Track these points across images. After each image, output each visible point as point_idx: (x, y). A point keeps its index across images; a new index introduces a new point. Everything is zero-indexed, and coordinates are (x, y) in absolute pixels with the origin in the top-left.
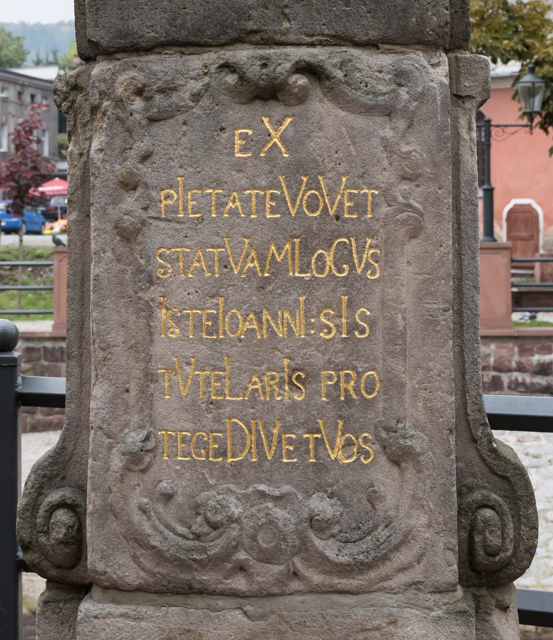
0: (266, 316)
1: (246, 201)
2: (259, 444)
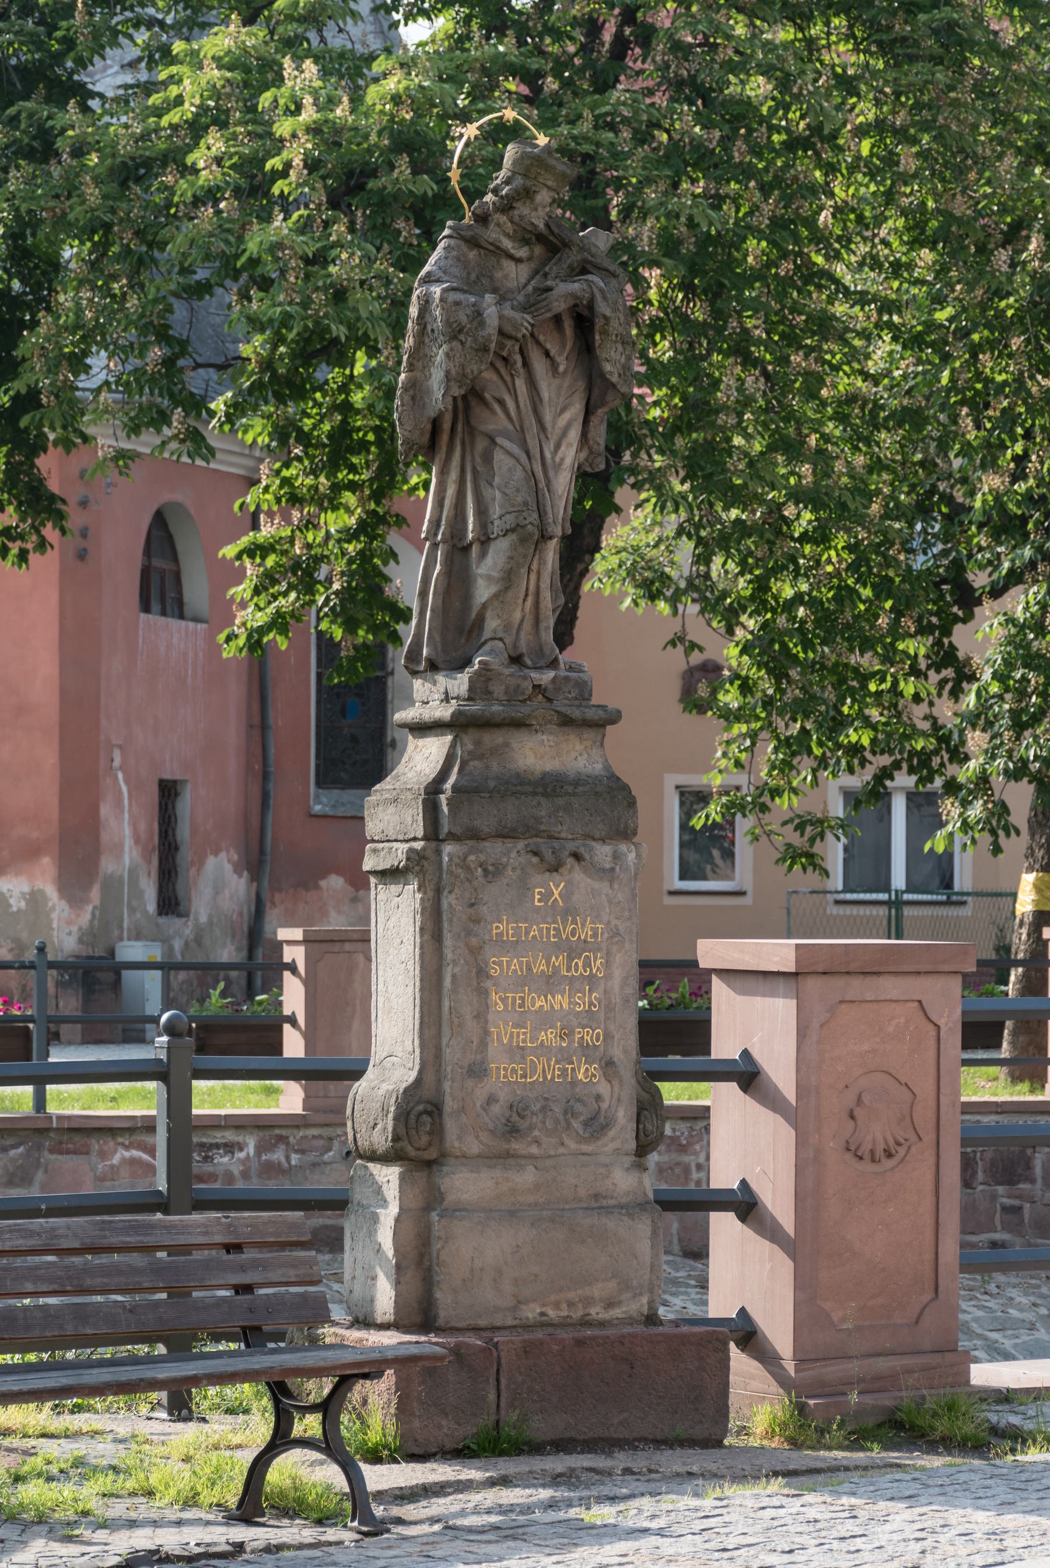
1: (540, 930)
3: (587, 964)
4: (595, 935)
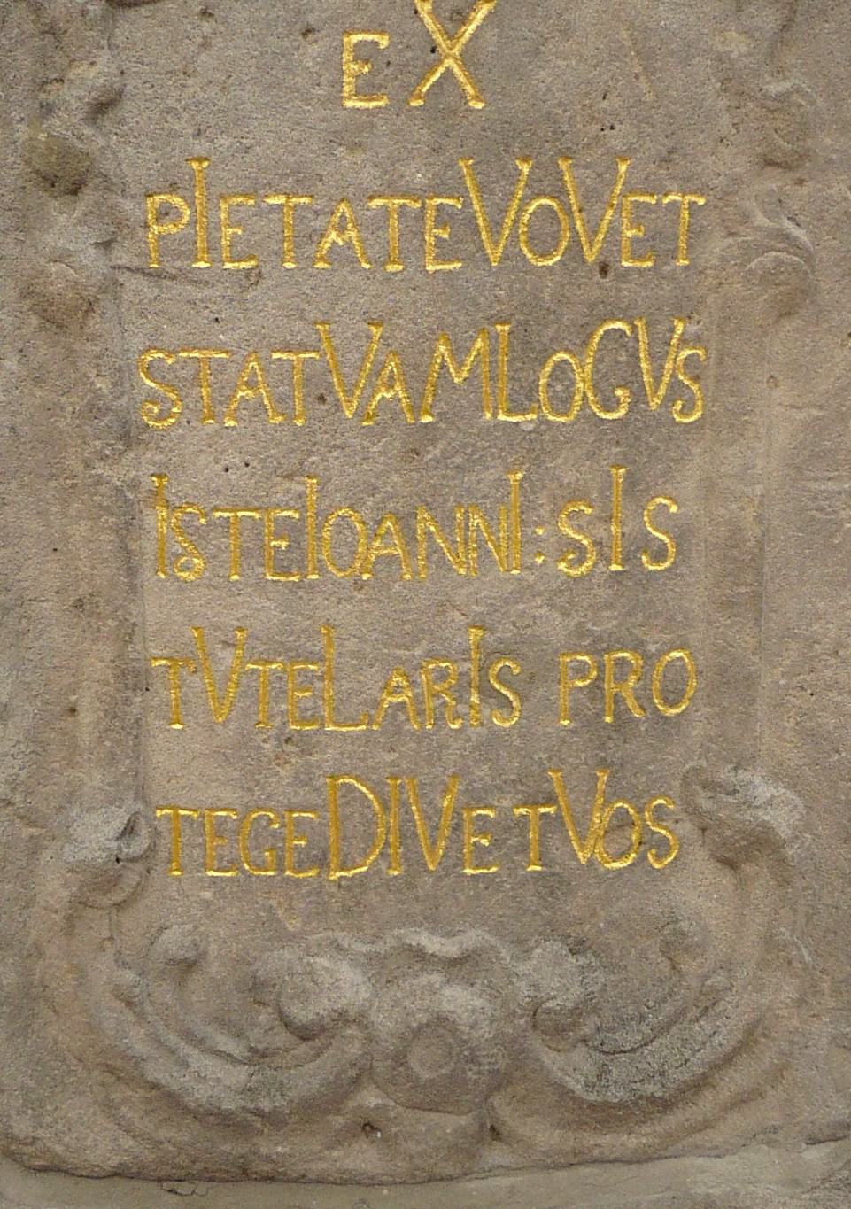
0: (425, 523)
2: (407, 835)
3: (618, 369)
4: (657, 243)
